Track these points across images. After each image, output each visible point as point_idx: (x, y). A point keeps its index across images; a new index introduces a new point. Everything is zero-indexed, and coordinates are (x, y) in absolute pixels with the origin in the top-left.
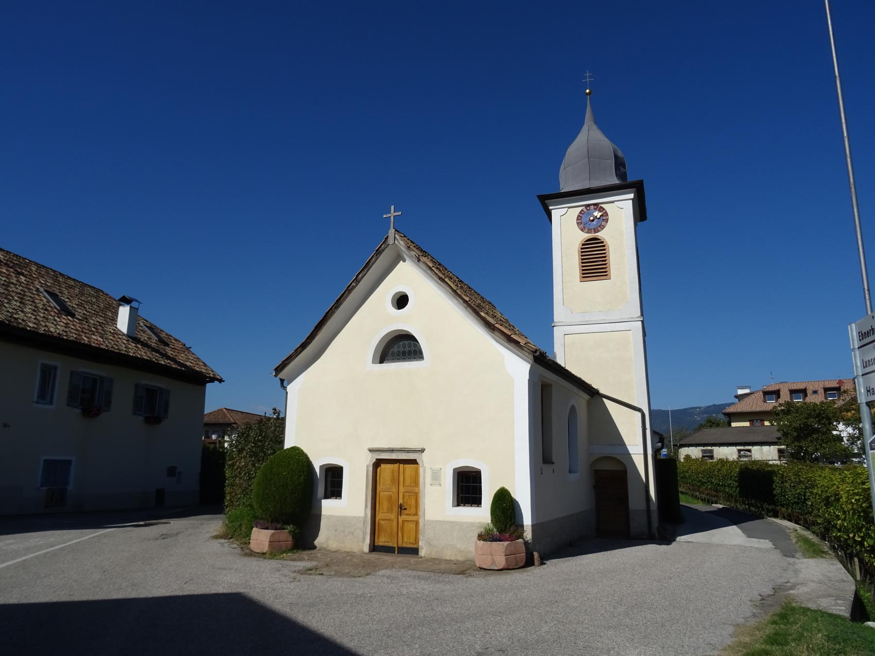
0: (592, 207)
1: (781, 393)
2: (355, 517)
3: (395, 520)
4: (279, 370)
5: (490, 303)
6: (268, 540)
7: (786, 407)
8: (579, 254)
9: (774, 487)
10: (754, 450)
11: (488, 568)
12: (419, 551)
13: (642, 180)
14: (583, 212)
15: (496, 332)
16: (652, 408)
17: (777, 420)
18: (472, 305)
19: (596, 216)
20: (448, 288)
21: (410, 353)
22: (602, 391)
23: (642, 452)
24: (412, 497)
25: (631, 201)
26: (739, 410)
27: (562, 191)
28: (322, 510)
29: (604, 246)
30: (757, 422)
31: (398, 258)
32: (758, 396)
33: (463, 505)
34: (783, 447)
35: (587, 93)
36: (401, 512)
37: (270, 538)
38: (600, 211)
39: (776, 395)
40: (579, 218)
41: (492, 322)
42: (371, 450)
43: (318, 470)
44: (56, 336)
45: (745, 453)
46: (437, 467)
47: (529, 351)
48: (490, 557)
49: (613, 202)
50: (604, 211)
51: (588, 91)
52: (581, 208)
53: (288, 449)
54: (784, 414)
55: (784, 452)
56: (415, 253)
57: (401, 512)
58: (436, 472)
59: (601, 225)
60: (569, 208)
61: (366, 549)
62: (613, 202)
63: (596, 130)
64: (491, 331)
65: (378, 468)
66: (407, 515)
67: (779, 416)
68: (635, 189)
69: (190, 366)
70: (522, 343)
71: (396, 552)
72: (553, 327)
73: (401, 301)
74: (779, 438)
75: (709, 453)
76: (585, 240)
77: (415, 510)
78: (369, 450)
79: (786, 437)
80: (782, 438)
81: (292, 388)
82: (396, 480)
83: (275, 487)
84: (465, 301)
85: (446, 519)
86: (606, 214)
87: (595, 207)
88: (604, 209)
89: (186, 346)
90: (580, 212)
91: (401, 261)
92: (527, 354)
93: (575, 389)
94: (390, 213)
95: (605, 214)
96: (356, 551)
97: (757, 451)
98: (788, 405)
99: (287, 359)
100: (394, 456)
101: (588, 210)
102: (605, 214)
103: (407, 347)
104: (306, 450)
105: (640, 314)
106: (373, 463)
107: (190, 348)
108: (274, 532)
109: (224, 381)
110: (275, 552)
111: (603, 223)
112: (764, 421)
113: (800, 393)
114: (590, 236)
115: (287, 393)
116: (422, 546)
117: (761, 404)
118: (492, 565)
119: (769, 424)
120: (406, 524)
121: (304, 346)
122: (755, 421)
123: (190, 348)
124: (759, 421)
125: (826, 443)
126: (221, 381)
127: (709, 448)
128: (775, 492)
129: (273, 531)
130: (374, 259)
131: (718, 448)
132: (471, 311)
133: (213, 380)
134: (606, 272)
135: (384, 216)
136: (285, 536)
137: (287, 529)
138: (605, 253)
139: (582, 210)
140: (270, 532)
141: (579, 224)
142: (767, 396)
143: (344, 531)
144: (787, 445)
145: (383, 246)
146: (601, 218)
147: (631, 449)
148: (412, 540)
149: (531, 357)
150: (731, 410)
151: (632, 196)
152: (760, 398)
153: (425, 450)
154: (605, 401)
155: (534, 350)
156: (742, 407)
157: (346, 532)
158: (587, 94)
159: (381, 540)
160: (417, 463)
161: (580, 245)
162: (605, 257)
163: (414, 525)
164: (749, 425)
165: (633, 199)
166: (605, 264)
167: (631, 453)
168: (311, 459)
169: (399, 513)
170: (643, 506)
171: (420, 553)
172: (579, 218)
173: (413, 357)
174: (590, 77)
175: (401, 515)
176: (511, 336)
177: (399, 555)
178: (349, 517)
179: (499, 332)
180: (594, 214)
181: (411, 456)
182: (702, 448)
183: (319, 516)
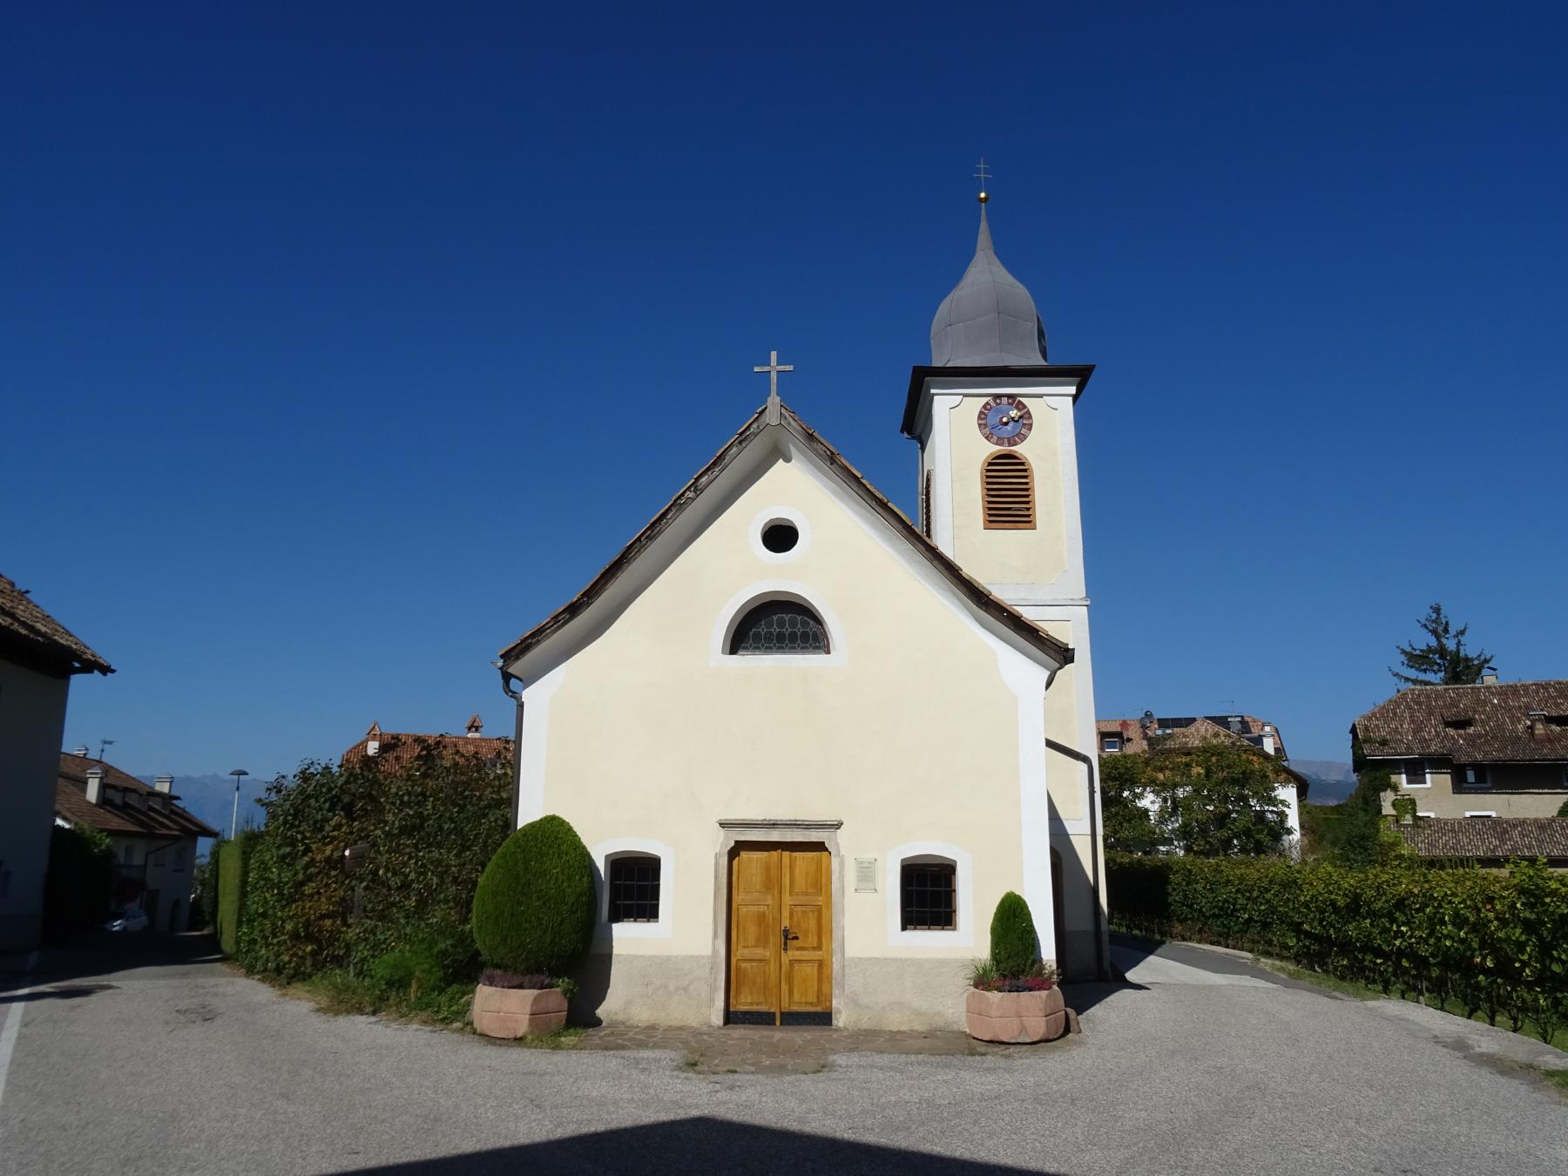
0: (1005, 400)
2: (691, 957)
3: (772, 960)
4: (510, 656)
6: (528, 1010)
9: (1170, 891)
12: (833, 1016)
20: (893, 522)
23: (1088, 831)
24: (810, 914)
25: (1071, 398)
28: (614, 944)
29: (1025, 470)
31: (776, 453)
33: (913, 927)
35: (981, 199)
36: (785, 944)
37: (532, 1005)
40: (983, 416)
42: (723, 825)
43: (601, 865)
46: (868, 856)
48: (1016, 1021)
49: (1040, 396)
50: (1026, 410)
51: (983, 195)
52: (985, 400)
53: (532, 826)
56: (824, 449)
57: (785, 944)
58: (866, 865)
59: (1020, 433)
61: (717, 1018)
62: (1040, 396)
65: (734, 859)
66: (799, 949)
69: (46, 632)
71: (778, 1023)
78: (720, 824)
81: (535, 697)
82: (771, 883)
83: (539, 899)
85: (892, 955)
86: (1028, 415)
87: (1010, 401)
88: (1025, 407)
89: (17, 587)
90: (984, 407)
91: (781, 460)
94: (769, 365)
96: (694, 1025)
99: (532, 635)
100: (775, 836)
101: (997, 404)
103: (799, 626)
106: (729, 848)
107: (27, 592)
108: (539, 995)
109: (113, 671)
110: (544, 1034)
114: (1000, 450)
115: (521, 705)
116: (838, 1009)
118: (1019, 1035)
120: (796, 966)
121: (573, 610)
123: (27, 592)
125: (1129, 821)
126: (106, 670)
128: (1170, 899)
129: (535, 992)
130: (734, 449)
133: (92, 666)
135: (756, 369)
136: (556, 999)
137: (558, 986)
139: (987, 403)
140: (530, 994)
141: (983, 427)
143: (666, 987)
145: (755, 426)
146: (1021, 420)
148: (812, 998)
153: (842, 824)
158: (981, 200)
159: (743, 1001)
162: (1027, 490)
163: (815, 969)
167: (1069, 833)
168: (585, 841)
169: (783, 946)
170: (1089, 925)
171: (834, 1022)
172: (983, 416)
174: (986, 171)
175: (785, 949)
177: (782, 1027)
178: (677, 957)
180: (1011, 413)
181: (814, 836)
183: (608, 958)
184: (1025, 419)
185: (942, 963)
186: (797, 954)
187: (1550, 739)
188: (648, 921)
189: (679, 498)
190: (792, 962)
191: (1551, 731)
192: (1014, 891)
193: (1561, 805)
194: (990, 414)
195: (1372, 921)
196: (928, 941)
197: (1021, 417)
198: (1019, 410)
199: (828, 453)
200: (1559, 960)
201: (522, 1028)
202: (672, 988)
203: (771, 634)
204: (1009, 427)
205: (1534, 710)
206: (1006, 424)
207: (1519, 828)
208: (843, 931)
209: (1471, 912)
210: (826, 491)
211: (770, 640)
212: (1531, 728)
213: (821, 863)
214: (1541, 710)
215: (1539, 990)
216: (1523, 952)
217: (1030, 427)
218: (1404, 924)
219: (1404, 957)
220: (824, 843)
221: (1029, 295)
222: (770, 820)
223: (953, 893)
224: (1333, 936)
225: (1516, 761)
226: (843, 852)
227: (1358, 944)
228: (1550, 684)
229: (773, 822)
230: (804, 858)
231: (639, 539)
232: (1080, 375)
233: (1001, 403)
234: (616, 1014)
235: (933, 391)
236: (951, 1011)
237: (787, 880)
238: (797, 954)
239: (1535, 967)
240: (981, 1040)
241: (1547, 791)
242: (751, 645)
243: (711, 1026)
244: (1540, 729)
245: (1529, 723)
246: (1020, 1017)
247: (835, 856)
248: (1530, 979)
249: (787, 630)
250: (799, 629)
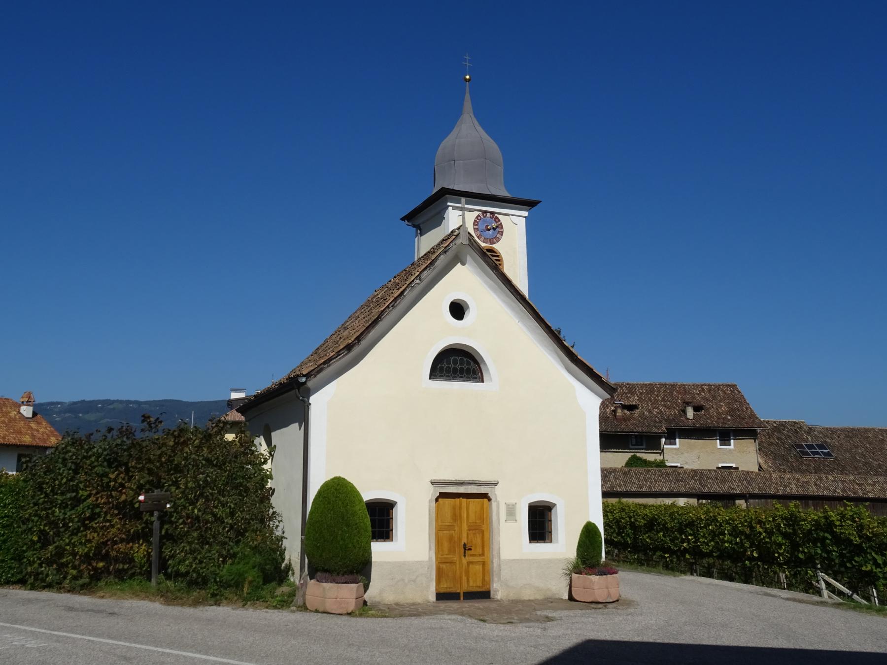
11: (604, 601)
21: (468, 371)
40: (476, 223)
42: (433, 483)
46: (512, 501)
49: (508, 215)
51: (468, 77)
52: (477, 213)
56: (492, 261)
57: (465, 553)
58: (510, 507)
61: (432, 598)
62: (508, 215)
71: (462, 598)
73: (458, 310)
77: (481, 550)
88: (499, 221)
90: (477, 217)
91: (459, 263)
100: (462, 490)
101: (484, 217)
103: (472, 370)
104: (349, 479)
111: (498, 236)
139: (479, 215)
143: (403, 580)
148: (479, 583)
157: (406, 581)
158: (466, 80)
160: (490, 500)
172: (476, 223)
173: (453, 375)
175: (465, 556)
178: (408, 562)
184: (498, 229)
185: (550, 561)
186: (472, 559)
187: (625, 419)
188: (385, 541)
189: (411, 283)
190: (469, 563)
191: (625, 414)
192: (591, 521)
193: (627, 459)
194: (480, 222)
195: (664, 534)
196: (541, 548)
197: (497, 227)
198: (497, 222)
199: (494, 264)
200: (803, 552)
201: (351, 608)
202: (406, 581)
203: (450, 368)
204: (491, 232)
205: (617, 401)
206: (489, 230)
207: (613, 474)
208: (499, 544)
209: (747, 529)
210: (485, 286)
211: (449, 372)
212: (614, 411)
213: (483, 505)
214: (620, 401)
215: (786, 567)
216: (781, 548)
217: (502, 233)
218: (691, 535)
219: (688, 553)
220: (487, 494)
221: (499, 149)
222: (459, 480)
223: (391, 520)
224: (629, 542)
225: (607, 432)
226: (498, 499)
227: (651, 546)
228: (623, 385)
229: (462, 482)
230: (474, 502)
231: (388, 307)
232: (528, 204)
233: (486, 216)
234: (374, 597)
235: (449, 204)
236: (554, 588)
237: (465, 515)
238: (472, 559)
239: (787, 556)
240: (584, 602)
241: (620, 450)
242: (458, 376)
243: (429, 602)
244: (619, 412)
245: (613, 408)
246: (608, 588)
247: (494, 502)
248: (782, 562)
249: (458, 366)
250: (465, 367)
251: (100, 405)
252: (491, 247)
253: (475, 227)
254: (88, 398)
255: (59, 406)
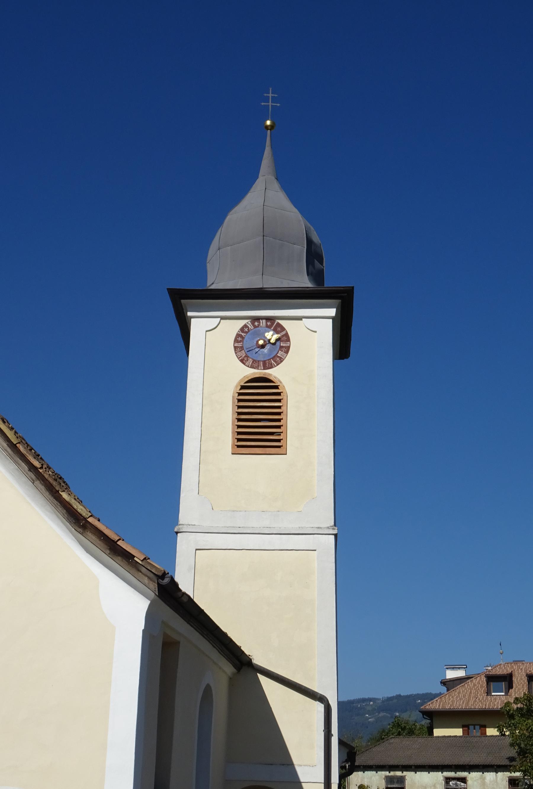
0: (263, 323)
1: (514, 679)
5: (61, 478)
7: (526, 705)
8: (233, 402)
10: (472, 779)
13: (353, 287)
14: (246, 330)
15: (89, 534)
16: (339, 701)
17: (510, 726)
18: (46, 476)
19: (269, 340)
22: (258, 660)
25: (331, 320)
26: (447, 707)
27: (213, 287)
29: (279, 394)
30: (475, 729)
32: (479, 683)
34: (518, 774)
38: (276, 331)
39: (507, 683)
40: (240, 339)
41: (82, 513)
44: (277, 96)
45: (456, 784)
47: (152, 575)
49: (300, 318)
50: (284, 333)
51: (268, 123)
52: (242, 323)
54: (522, 715)
55: (518, 784)
59: (276, 356)
60: (223, 318)
62: (300, 318)
63: (279, 190)
64: (79, 530)
67: (514, 719)
68: (340, 300)
70: (139, 557)
72: (177, 533)
74: (512, 759)
75: (398, 782)
76: (247, 380)
79: (525, 757)
80: (518, 759)
84: (32, 468)
88: (283, 329)
90: (242, 330)
92: (146, 580)
93: (213, 654)
95: (285, 338)
97: (475, 781)
98: (529, 701)
101: (255, 327)
102: (285, 338)
105: (332, 523)
112: (484, 727)
113: (502, 681)
117: (483, 698)
119: (498, 734)
122: (471, 727)
124: (477, 727)
127: (399, 773)
131: (413, 773)
132: (43, 488)
134: (279, 441)
138: (279, 407)
139: (245, 326)
142: (492, 684)
144: (525, 772)
146: (278, 343)
147: (303, 774)
149: (154, 586)
150: (434, 705)
151: (332, 312)
152: (482, 687)
154: (262, 679)
155: (160, 574)
156: (453, 701)
158: (267, 127)
161: (236, 387)
164: (461, 734)
165: (333, 319)
166: (279, 427)
167: (302, 780)
172: (240, 339)
174: (274, 100)
176: (118, 543)
179: (94, 534)
180: (266, 334)
182: (387, 773)
194: (247, 337)
217: (287, 350)
251: (419, 701)
252: (265, 374)
253: (236, 345)
254: (404, 693)
255: (371, 703)
